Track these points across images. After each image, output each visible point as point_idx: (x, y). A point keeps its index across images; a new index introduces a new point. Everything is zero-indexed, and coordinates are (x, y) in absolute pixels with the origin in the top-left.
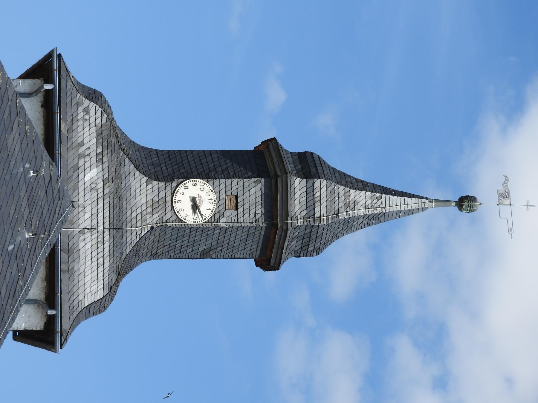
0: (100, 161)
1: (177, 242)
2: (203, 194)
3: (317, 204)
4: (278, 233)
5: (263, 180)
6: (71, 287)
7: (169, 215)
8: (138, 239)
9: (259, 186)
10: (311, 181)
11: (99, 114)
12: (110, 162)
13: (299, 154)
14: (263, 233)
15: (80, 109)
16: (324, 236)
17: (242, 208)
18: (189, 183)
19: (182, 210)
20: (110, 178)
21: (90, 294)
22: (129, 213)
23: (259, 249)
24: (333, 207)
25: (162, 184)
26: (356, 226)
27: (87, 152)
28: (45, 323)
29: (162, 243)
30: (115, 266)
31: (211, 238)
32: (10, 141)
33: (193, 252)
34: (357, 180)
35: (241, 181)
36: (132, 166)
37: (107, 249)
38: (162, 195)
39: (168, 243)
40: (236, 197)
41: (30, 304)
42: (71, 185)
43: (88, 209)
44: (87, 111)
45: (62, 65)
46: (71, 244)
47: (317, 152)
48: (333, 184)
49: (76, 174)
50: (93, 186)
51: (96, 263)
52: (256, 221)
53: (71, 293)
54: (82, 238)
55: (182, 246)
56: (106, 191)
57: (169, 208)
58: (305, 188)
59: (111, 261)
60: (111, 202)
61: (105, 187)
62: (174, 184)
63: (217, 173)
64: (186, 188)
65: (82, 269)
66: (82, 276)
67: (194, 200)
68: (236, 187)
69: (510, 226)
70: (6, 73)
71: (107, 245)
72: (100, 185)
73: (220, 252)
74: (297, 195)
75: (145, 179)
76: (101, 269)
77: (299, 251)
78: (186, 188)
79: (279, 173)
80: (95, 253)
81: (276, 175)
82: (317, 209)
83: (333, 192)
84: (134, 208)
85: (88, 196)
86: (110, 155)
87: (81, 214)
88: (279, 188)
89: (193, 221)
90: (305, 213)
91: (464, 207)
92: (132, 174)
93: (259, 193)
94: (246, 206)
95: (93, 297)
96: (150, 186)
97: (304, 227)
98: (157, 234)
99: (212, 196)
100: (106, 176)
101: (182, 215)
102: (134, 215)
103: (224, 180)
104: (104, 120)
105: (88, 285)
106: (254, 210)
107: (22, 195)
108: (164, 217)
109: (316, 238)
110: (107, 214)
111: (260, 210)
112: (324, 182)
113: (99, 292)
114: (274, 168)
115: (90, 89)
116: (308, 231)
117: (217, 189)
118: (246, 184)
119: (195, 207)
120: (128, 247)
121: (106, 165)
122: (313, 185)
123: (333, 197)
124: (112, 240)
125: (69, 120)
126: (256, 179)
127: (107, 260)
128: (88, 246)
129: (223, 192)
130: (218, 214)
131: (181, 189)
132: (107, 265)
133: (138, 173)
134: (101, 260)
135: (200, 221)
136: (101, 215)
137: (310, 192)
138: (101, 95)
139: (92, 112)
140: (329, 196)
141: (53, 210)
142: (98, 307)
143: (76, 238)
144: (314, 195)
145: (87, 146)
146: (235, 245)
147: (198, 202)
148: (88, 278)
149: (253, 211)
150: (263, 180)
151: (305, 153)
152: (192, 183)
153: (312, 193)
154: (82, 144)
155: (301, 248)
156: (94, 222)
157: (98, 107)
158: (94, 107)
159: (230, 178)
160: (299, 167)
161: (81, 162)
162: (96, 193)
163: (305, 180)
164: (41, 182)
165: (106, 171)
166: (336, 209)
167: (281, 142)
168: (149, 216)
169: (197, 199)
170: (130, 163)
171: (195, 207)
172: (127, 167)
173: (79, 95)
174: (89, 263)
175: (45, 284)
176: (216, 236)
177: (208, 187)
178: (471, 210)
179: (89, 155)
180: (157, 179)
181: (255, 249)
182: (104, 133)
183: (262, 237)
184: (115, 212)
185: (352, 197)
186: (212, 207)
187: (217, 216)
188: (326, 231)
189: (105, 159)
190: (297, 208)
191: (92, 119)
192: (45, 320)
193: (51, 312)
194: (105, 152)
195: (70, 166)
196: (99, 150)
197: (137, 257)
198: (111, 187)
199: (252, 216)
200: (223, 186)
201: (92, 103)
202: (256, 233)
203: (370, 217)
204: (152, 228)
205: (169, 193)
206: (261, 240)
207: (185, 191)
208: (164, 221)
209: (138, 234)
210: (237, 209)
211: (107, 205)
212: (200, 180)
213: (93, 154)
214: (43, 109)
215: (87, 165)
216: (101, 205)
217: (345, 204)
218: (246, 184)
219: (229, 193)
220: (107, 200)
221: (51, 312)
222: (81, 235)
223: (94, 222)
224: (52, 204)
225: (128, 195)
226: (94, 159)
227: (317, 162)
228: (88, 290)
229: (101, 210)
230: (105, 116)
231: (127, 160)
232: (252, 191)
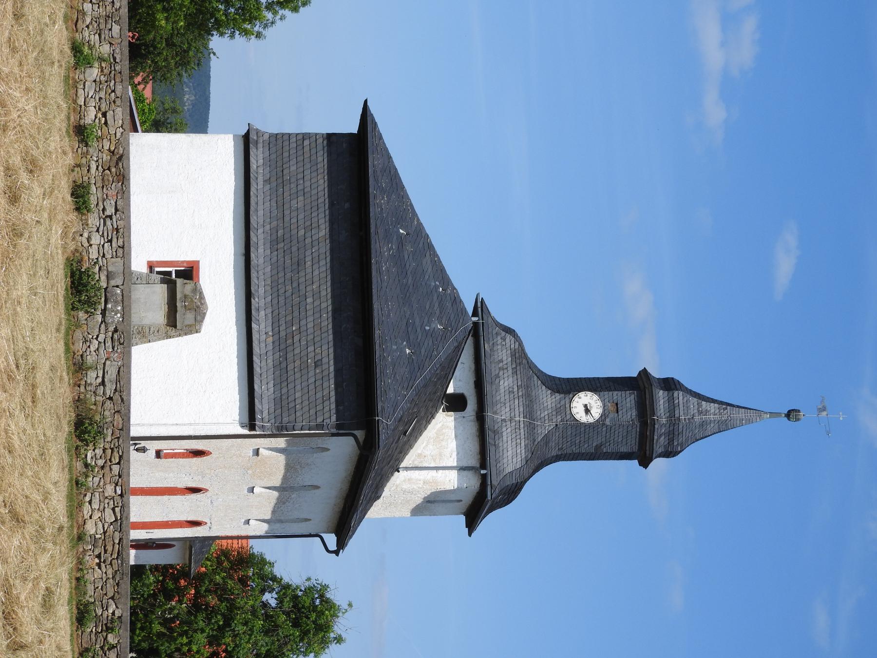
0: (515, 372)
1: (576, 439)
2: (593, 403)
3: (677, 408)
4: (649, 428)
5: (635, 392)
6: (497, 457)
7: (568, 417)
8: (546, 432)
9: (633, 396)
10: (671, 393)
11: (513, 342)
12: (522, 374)
13: (664, 379)
14: (638, 430)
15: (499, 338)
16: (684, 433)
17: (621, 411)
18: (582, 394)
19: (577, 413)
20: (523, 385)
21: (511, 464)
22: (539, 413)
23: (637, 443)
24: (689, 411)
25: (562, 395)
26: (709, 429)
27: (505, 366)
28: (481, 484)
29: (565, 439)
30: (529, 446)
31: (600, 435)
32: (424, 263)
33: (589, 447)
34: (708, 398)
35: (619, 393)
36: (540, 382)
37: (522, 434)
38: (563, 403)
39: (570, 439)
40: (617, 404)
41: (469, 470)
42: (494, 387)
43: (508, 405)
44: (504, 339)
45: (484, 305)
46: (496, 427)
47: (676, 377)
48: (688, 396)
49: (497, 380)
50: (510, 389)
51: (514, 443)
52: (632, 421)
53: (497, 461)
54: (504, 424)
55: (580, 442)
56: (520, 394)
57: (569, 412)
58: (667, 398)
59: (527, 442)
60: (524, 402)
61: (519, 391)
62: (571, 396)
63: (602, 388)
64: (580, 398)
65: (505, 446)
66: (505, 451)
67: (586, 406)
68: (616, 397)
69: (828, 429)
70: (419, 220)
71: (522, 431)
72: (516, 389)
73: (609, 447)
74: (662, 402)
75: (549, 392)
76: (519, 447)
77: (667, 445)
78: (580, 398)
79: (647, 386)
80: (514, 436)
81: (645, 387)
82: (677, 412)
83: (688, 401)
84: (542, 411)
85: (507, 396)
86: (522, 370)
87: (503, 408)
88: (647, 396)
89: (586, 420)
90: (668, 414)
91: (791, 416)
92: (540, 387)
93: (633, 402)
94: (624, 410)
95: (514, 466)
96: (554, 397)
97: (668, 425)
98: (561, 431)
99: (599, 403)
100: (520, 383)
101: (577, 417)
102: (542, 415)
103: (607, 392)
104: (517, 346)
105: (510, 458)
106: (630, 413)
107: (435, 300)
108: (565, 419)
109: (678, 434)
110: (521, 409)
111: (634, 413)
112: (681, 393)
113: (518, 463)
114: (644, 384)
115: (506, 326)
116: (671, 428)
117: (603, 399)
118: (623, 395)
119: (587, 411)
120: (539, 437)
121: (519, 376)
122: (673, 395)
123: (689, 405)
124: (526, 428)
125: (491, 343)
126: (631, 392)
127: (523, 442)
128: (509, 430)
129: (607, 400)
130: (604, 416)
131: (576, 398)
132: (523, 444)
133: (544, 387)
134: (518, 441)
135: (591, 420)
136: (517, 409)
137: (671, 400)
138: (514, 331)
139: (508, 340)
140: (685, 404)
141: (458, 320)
142: (519, 475)
143: (500, 424)
144: (674, 402)
145: (505, 362)
146: (619, 441)
147: (589, 408)
148: (510, 453)
149: (629, 414)
150: (635, 392)
151: (667, 379)
152: (584, 394)
153: (673, 401)
154: (501, 361)
155: (669, 443)
156: (513, 414)
157: (511, 337)
158: (509, 337)
159: (611, 391)
160: (663, 385)
161: (501, 373)
162: (513, 395)
163: (667, 392)
164: (448, 298)
165: (519, 380)
166: (692, 413)
167: (649, 370)
168: (553, 417)
169: (588, 405)
170: (538, 379)
171: (587, 411)
172: (536, 382)
173: (497, 328)
174: (510, 442)
175: (479, 456)
176: (604, 433)
177: (595, 397)
178: (798, 420)
179: (507, 368)
180: (558, 392)
181: (634, 444)
182: (517, 355)
183: (638, 433)
184: (528, 410)
185: (704, 406)
186: (600, 411)
187: (603, 418)
188: (685, 429)
189: (518, 372)
190: (662, 411)
191: (508, 345)
192: (480, 482)
193: (483, 472)
194: (518, 368)
195: (493, 374)
196: (514, 366)
197: (547, 448)
198: (524, 392)
199: (629, 417)
200: (606, 396)
201: (507, 334)
202: (633, 430)
203: (720, 422)
204: (557, 425)
205: (567, 401)
206: (638, 436)
207: (579, 400)
208: (565, 421)
209: (546, 428)
210: (618, 412)
211: (521, 404)
212: (590, 393)
213: (510, 369)
214: (473, 338)
215: (506, 375)
216: (516, 402)
217: (698, 411)
218: (623, 395)
219: (611, 401)
220: (521, 400)
221: (483, 472)
222: (503, 422)
223: (513, 414)
224: (456, 316)
225: (537, 401)
226: (510, 371)
227: (677, 384)
228: (510, 461)
229: (517, 406)
230: (517, 343)
231: (536, 377)
232: (628, 400)
